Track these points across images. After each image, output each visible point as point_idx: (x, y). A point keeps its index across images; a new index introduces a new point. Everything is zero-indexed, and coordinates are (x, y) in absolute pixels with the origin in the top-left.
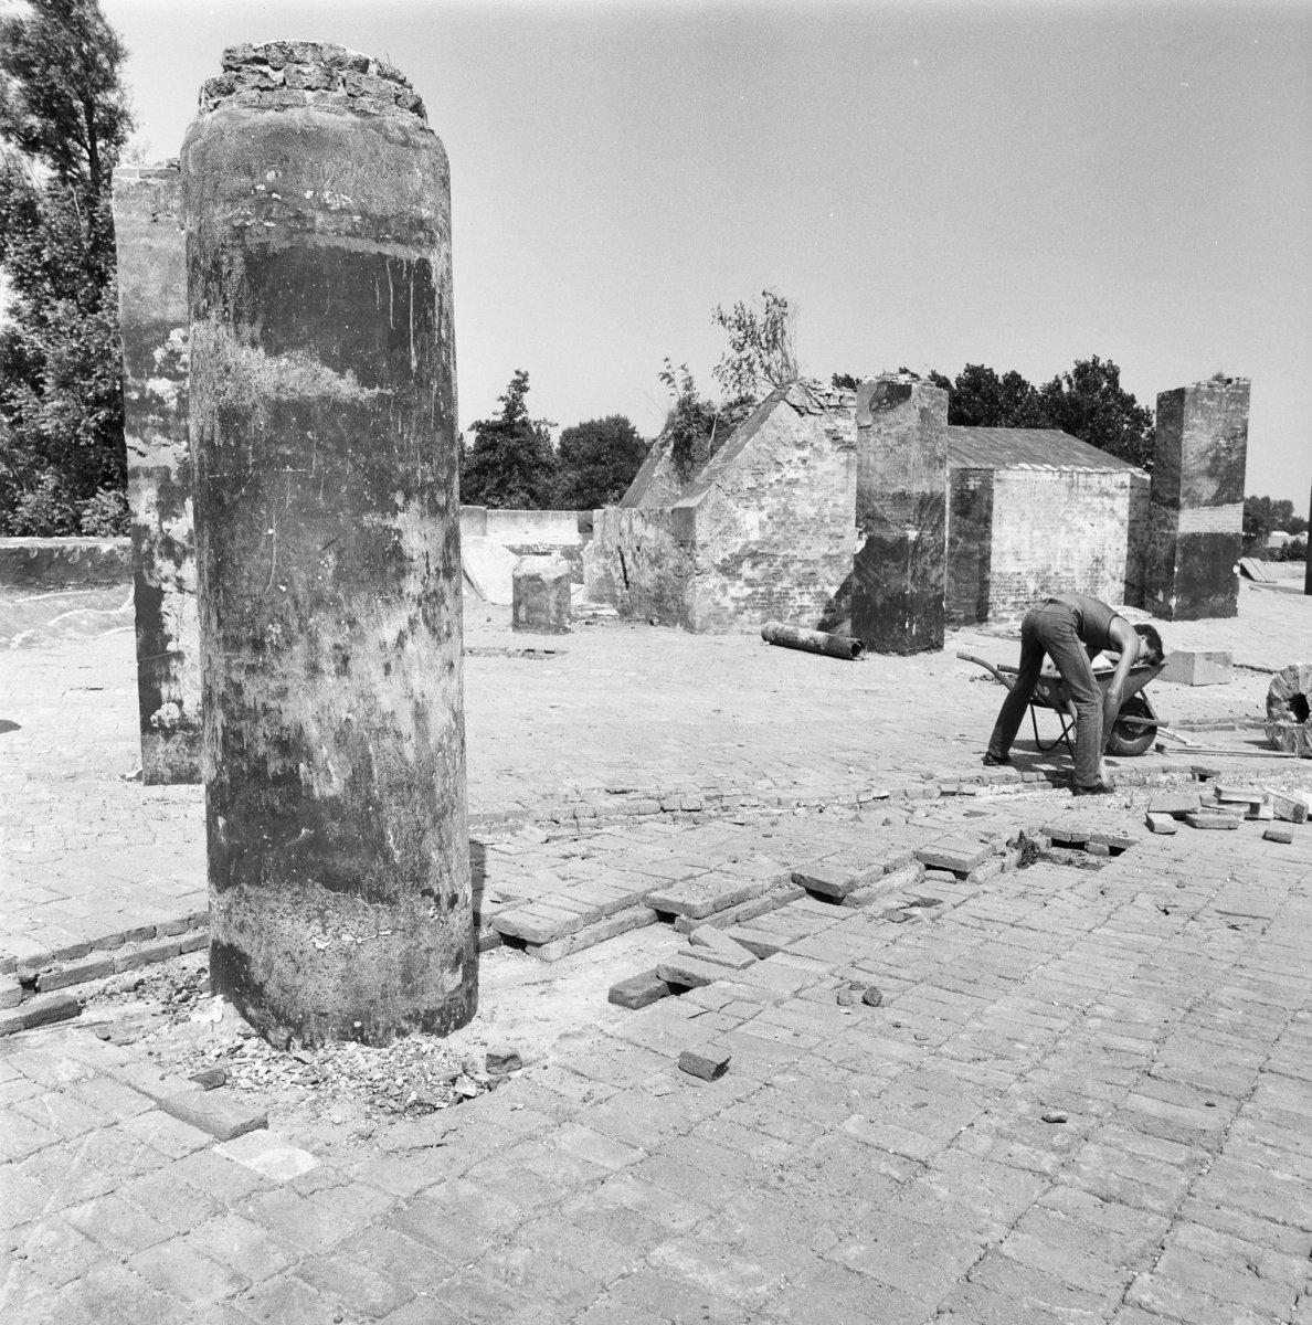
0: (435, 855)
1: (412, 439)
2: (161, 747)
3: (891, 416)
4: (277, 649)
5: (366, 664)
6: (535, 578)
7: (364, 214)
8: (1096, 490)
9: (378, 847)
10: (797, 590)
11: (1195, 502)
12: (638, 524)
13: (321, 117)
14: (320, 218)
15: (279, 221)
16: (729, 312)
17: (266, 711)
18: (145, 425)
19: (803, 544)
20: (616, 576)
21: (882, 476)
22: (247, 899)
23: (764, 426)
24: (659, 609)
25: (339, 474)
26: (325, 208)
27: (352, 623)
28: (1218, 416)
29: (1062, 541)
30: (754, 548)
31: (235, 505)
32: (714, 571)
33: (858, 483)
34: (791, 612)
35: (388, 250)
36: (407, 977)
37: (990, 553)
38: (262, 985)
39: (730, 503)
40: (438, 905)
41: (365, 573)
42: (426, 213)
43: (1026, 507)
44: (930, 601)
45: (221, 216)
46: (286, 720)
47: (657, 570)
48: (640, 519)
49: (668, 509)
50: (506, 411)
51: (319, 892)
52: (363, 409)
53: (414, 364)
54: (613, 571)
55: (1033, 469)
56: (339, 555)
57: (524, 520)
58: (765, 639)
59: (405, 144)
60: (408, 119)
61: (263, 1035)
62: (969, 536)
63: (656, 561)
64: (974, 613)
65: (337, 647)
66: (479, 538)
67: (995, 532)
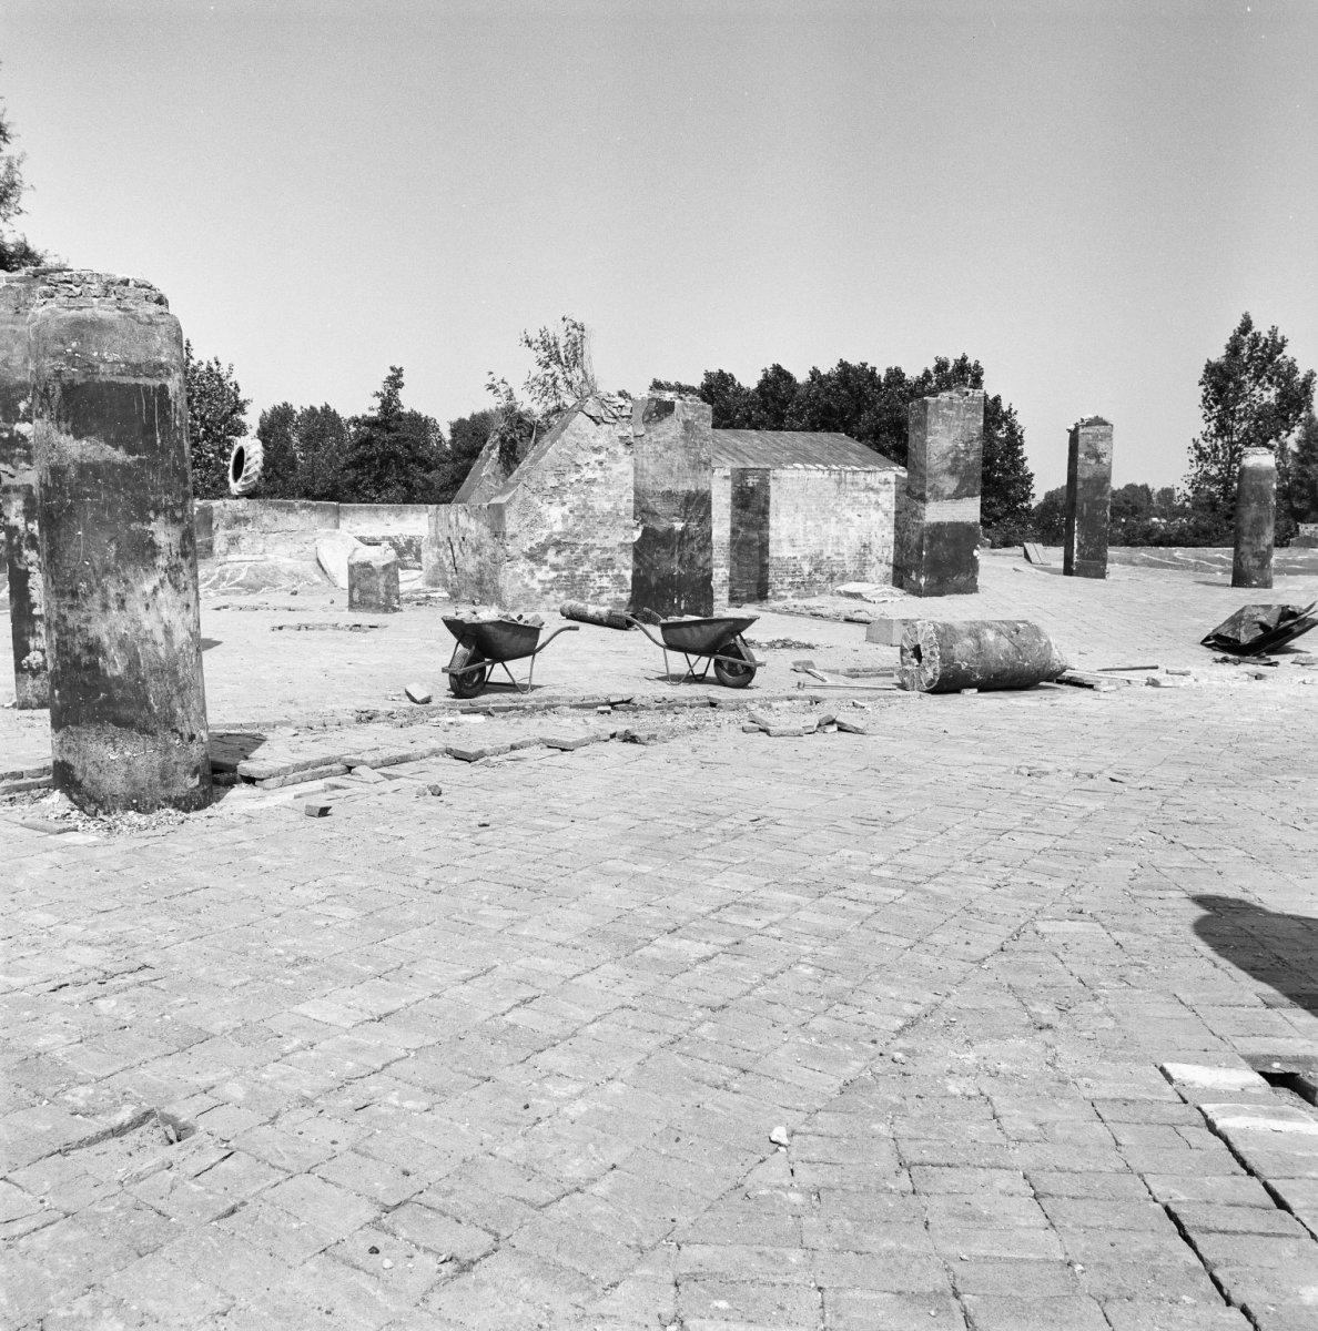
0: (179, 710)
1: (158, 482)
2: (30, 683)
3: (660, 427)
4: (85, 596)
5: (135, 604)
6: (366, 565)
7: (126, 363)
8: (862, 486)
9: (145, 703)
10: (596, 573)
11: (939, 495)
12: (462, 517)
13: (101, 313)
14: (102, 366)
15: (79, 368)
16: (534, 335)
17: (80, 630)
18: (13, 456)
19: (601, 534)
20: (447, 562)
21: (653, 477)
22: (72, 734)
23: (564, 434)
24: (480, 591)
25: (117, 502)
26: (104, 361)
27: (126, 581)
28: (957, 423)
29: (832, 529)
30: (558, 538)
31: (60, 518)
32: (523, 558)
33: (635, 483)
34: (592, 592)
35: (141, 382)
36: (163, 777)
37: (768, 541)
38: (81, 781)
39: (536, 500)
40: (182, 738)
41: (133, 555)
42: (163, 359)
43: (800, 501)
44: (697, 581)
45: (49, 365)
46: (91, 634)
47: (478, 558)
48: (464, 513)
49: (485, 505)
50: (382, 406)
51: (112, 728)
52: (130, 468)
53: (159, 441)
54: (444, 557)
55: (806, 469)
56: (118, 545)
57: (386, 513)
58: (563, 614)
59: (150, 324)
60: (153, 309)
61: (82, 809)
62: (749, 526)
63: (477, 550)
64: (755, 592)
65: (118, 594)
66: (332, 530)
67: (772, 522)
